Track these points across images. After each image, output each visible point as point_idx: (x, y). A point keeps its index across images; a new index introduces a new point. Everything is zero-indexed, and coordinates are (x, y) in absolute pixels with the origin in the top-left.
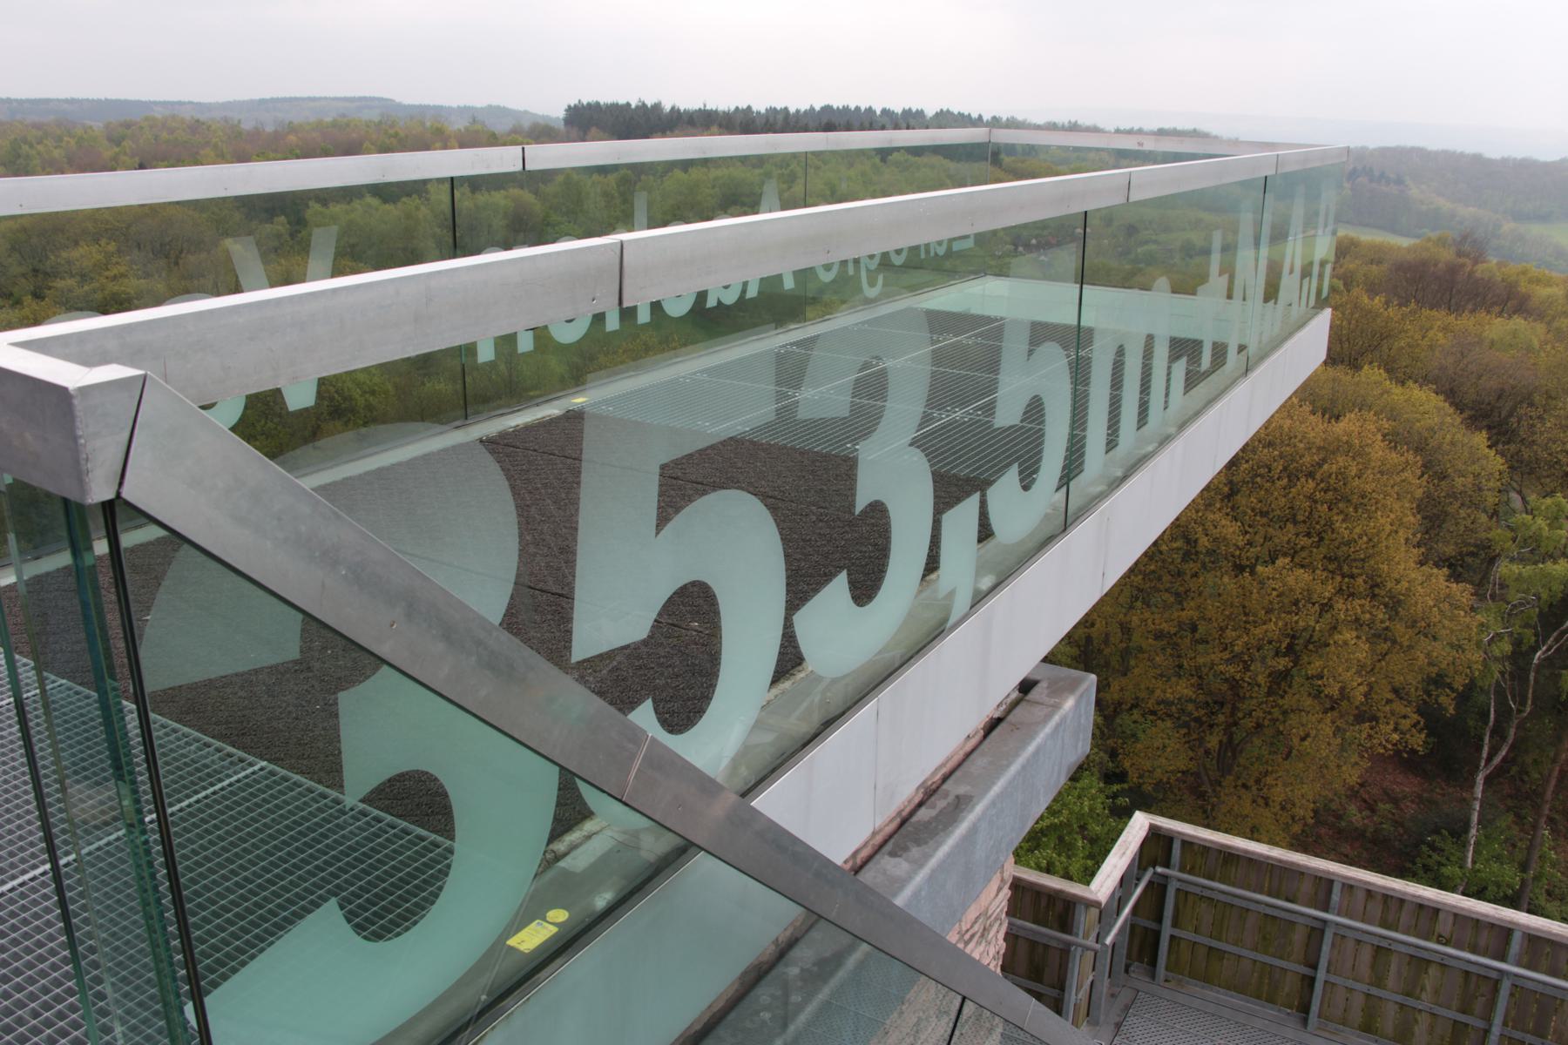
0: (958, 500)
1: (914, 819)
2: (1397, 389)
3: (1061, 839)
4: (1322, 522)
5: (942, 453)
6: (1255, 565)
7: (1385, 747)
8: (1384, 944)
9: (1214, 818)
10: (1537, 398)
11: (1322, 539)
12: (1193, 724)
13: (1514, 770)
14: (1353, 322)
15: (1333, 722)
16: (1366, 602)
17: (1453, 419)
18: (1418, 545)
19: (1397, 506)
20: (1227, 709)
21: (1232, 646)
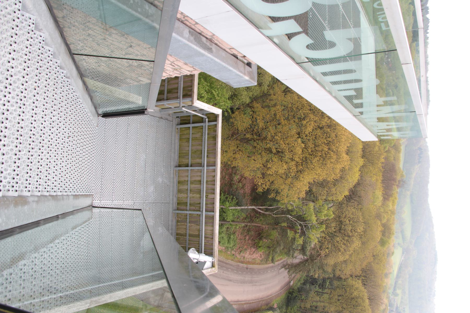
0: (300, 25)
1: (202, 37)
2: (358, 169)
3: (211, 99)
4: (316, 155)
5: (314, 25)
6: (301, 138)
7: (256, 182)
8: (202, 182)
9: (227, 140)
10: (360, 206)
11: (311, 155)
12: (252, 129)
13: (258, 215)
14: (376, 154)
15: (260, 167)
16: (295, 170)
17: (351, 186)
18: (314, 181)
19: (324, 174)
20: (258, 138)
21: (276, 136)
